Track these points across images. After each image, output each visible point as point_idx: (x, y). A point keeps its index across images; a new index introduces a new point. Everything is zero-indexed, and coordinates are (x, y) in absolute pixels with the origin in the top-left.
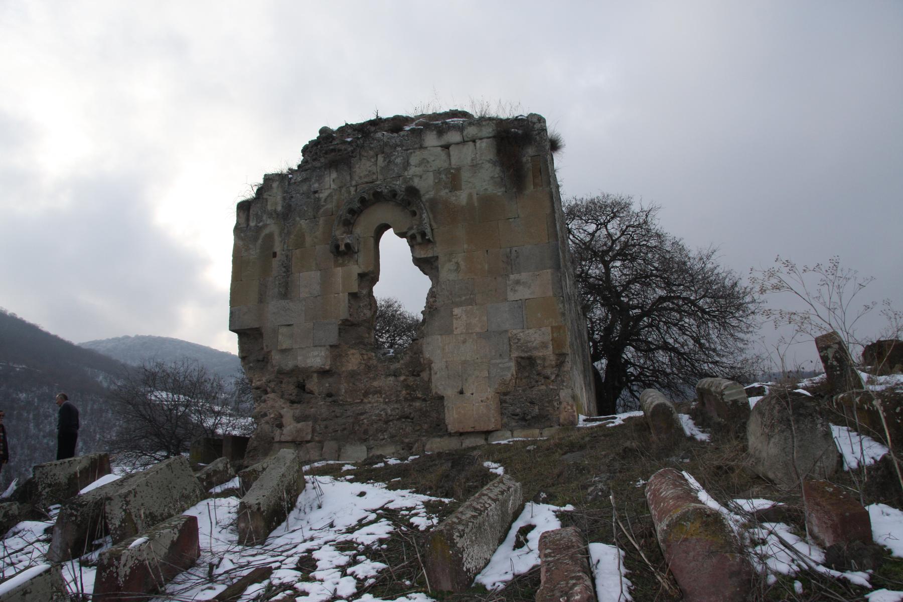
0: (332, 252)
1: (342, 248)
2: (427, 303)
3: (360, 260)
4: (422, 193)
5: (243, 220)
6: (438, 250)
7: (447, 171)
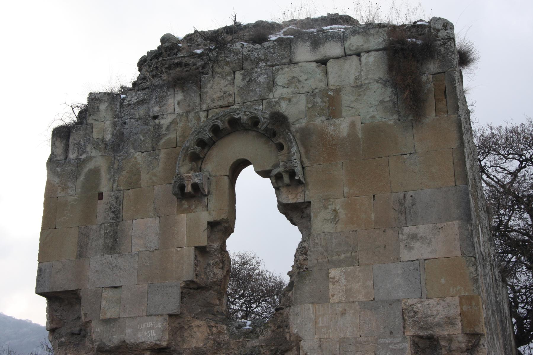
1: (189, 189)
2: (296, 261)
4: (291, 120)
5: (60, 151)
6: (311, 194)
7: (324, 93)
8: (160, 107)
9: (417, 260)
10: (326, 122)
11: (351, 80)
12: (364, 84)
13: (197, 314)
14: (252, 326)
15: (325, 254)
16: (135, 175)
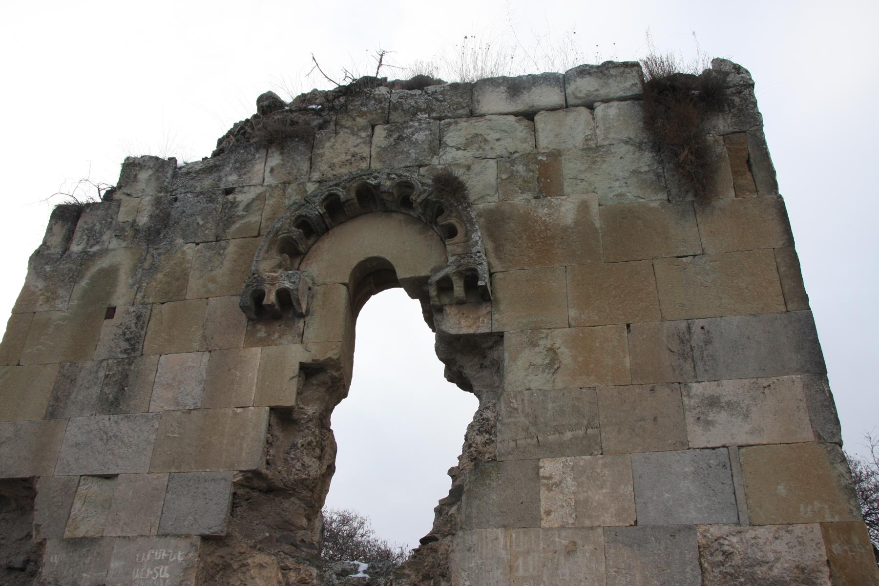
1: (271, 298)
5: (57, 240)
6: (504, 318)
7: (530, 158)
8: (239, 176)
9: (724, 446)
10: (533, 201)
11: (579, 139)
12: (602, 146)
13: (260, 542)
14: (369, 574)
15: (532, 429)
16: (178, 280)
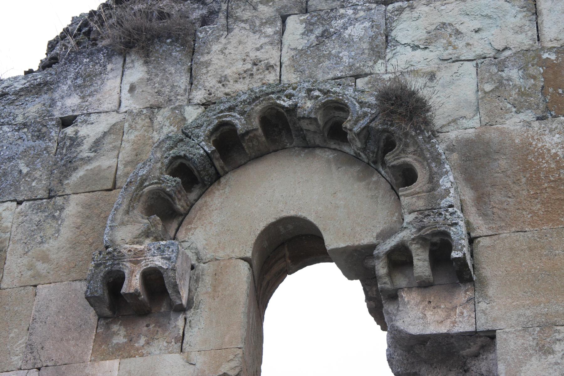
0: (92, 300)
1: (133, 283)
3: (194, 337)
8: (83, 98)
10: (536, 124)
